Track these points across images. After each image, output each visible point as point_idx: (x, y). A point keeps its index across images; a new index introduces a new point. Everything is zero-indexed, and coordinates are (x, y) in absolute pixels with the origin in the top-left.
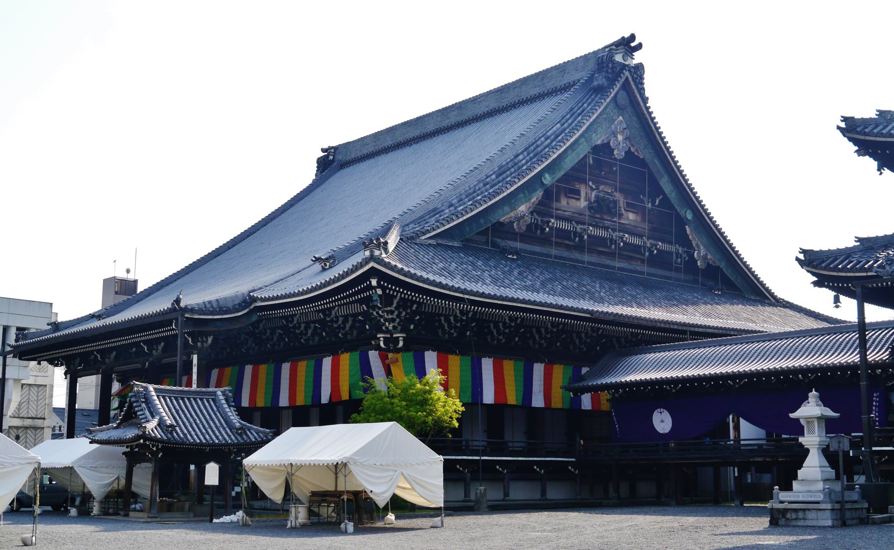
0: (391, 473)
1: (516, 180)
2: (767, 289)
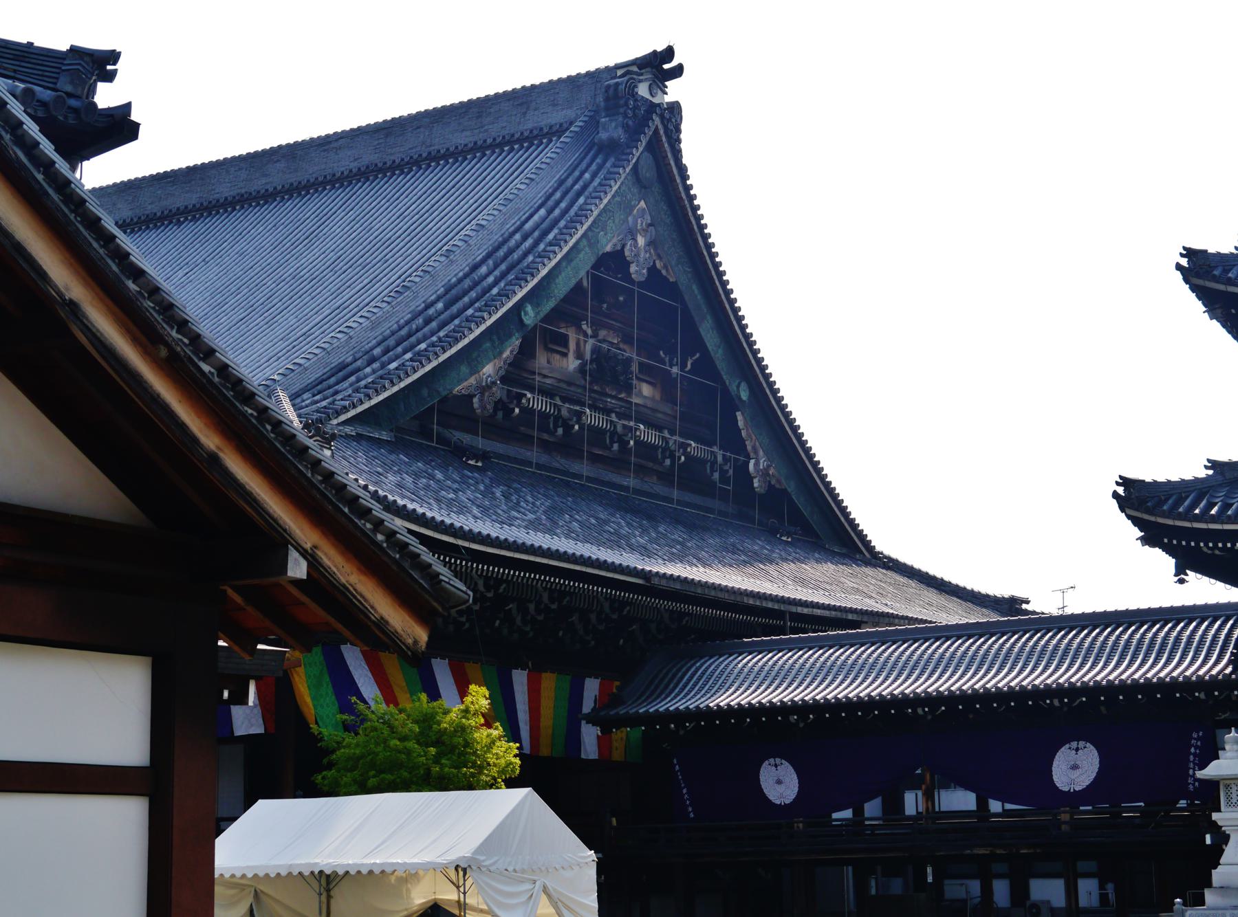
0: (528, 886)
1: (485, 315)
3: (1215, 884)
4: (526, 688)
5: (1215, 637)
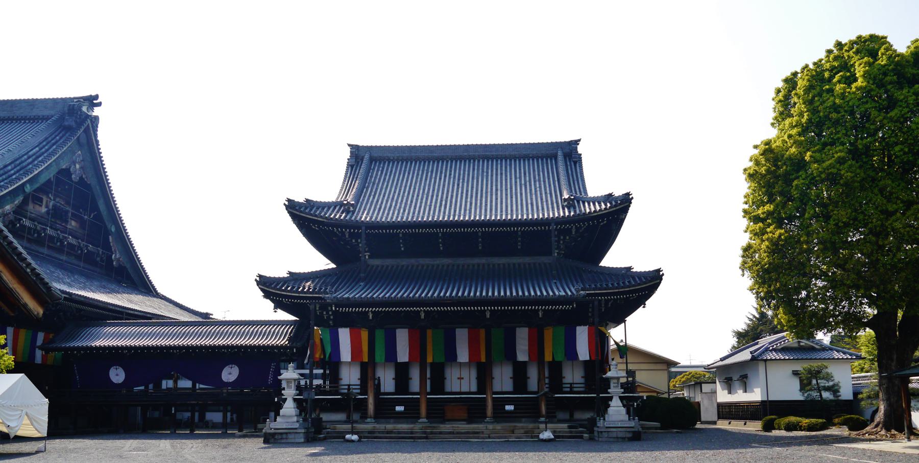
2: (153, 287)
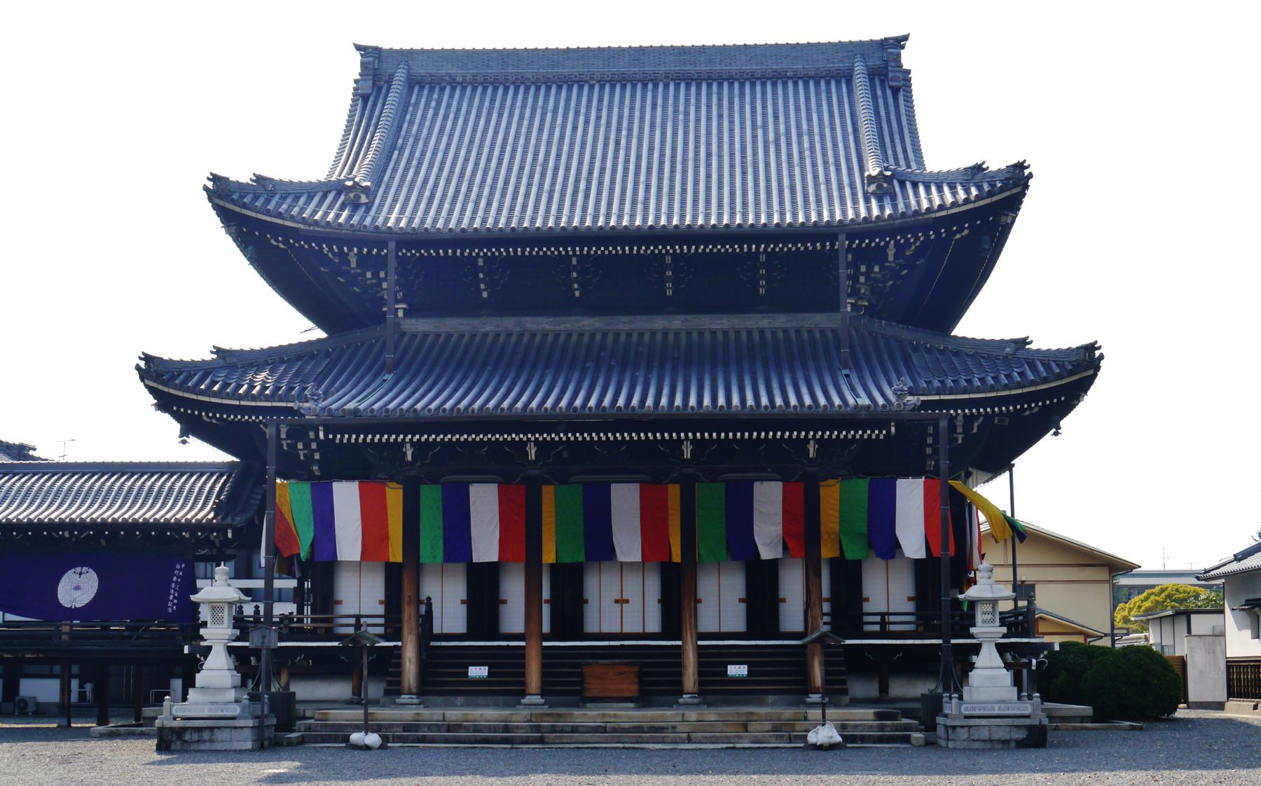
3: (197, 684)
4: (440, 503)
5: (201, 489)
